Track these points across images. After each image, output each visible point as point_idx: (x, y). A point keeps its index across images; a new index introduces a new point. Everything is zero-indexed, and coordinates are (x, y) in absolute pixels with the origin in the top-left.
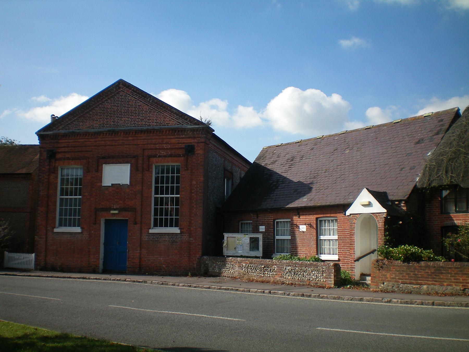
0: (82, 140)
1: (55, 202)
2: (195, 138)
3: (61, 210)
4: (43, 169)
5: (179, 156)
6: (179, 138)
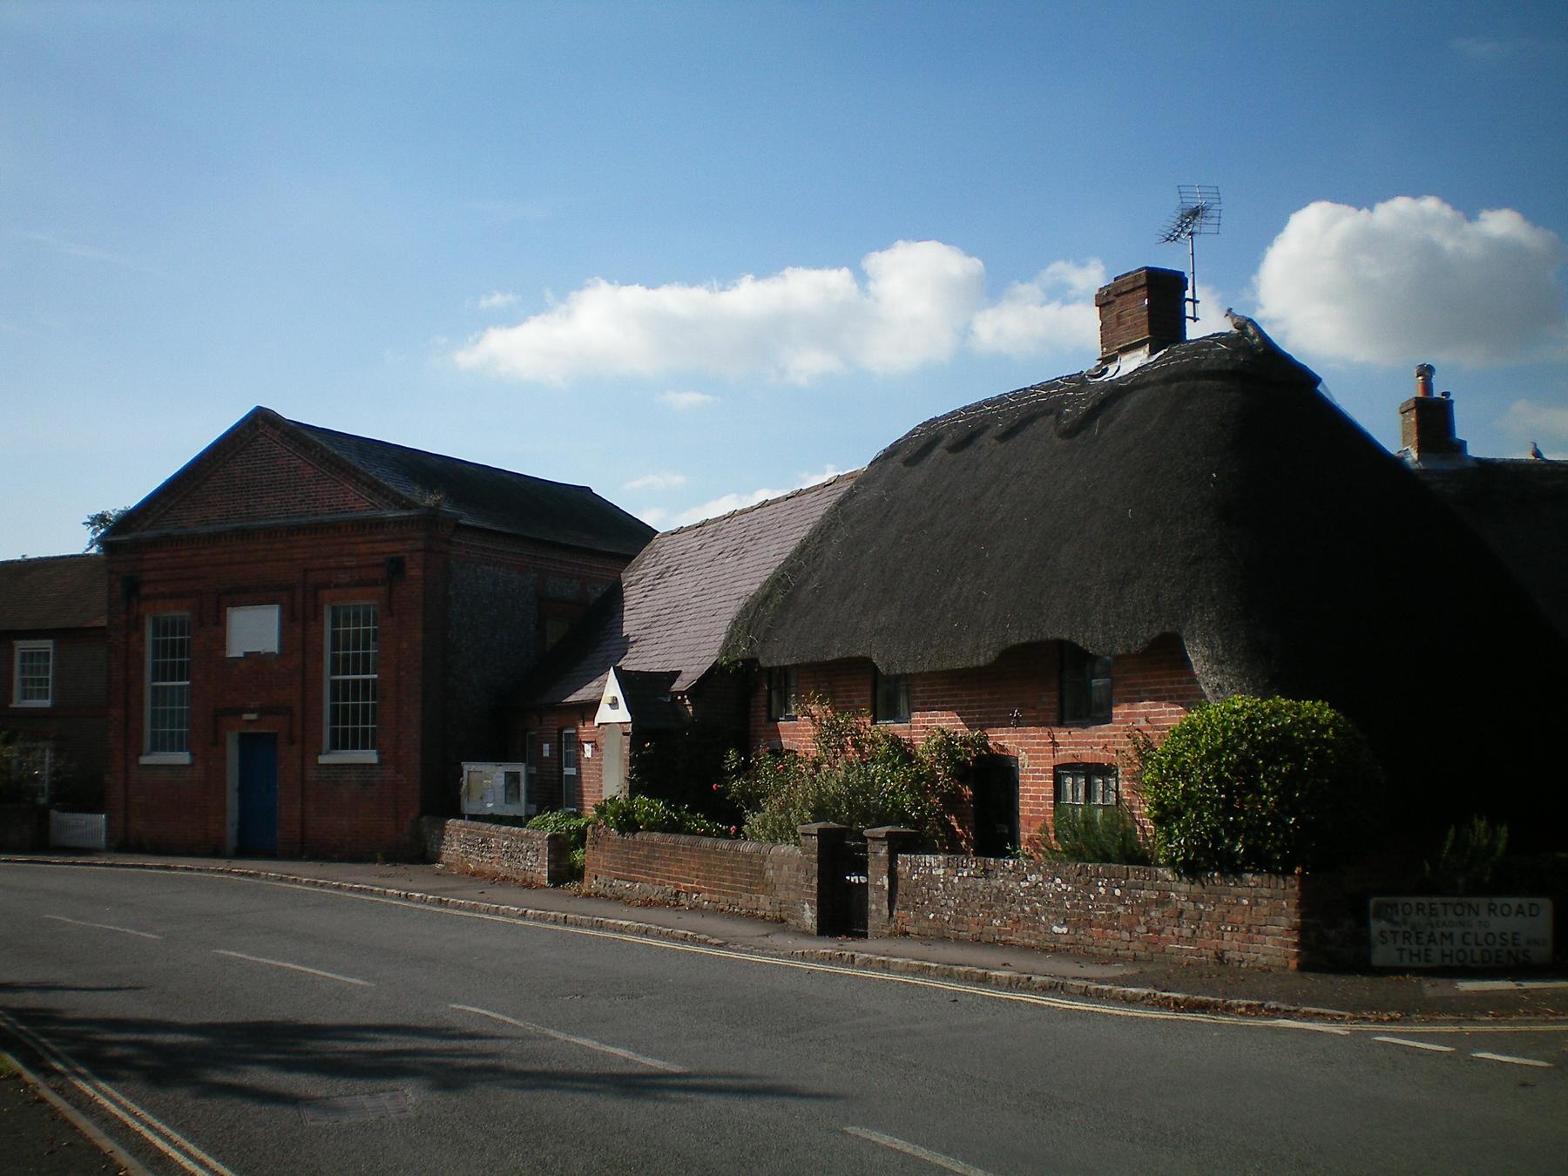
1: (141, 695)
3: (334, 709)
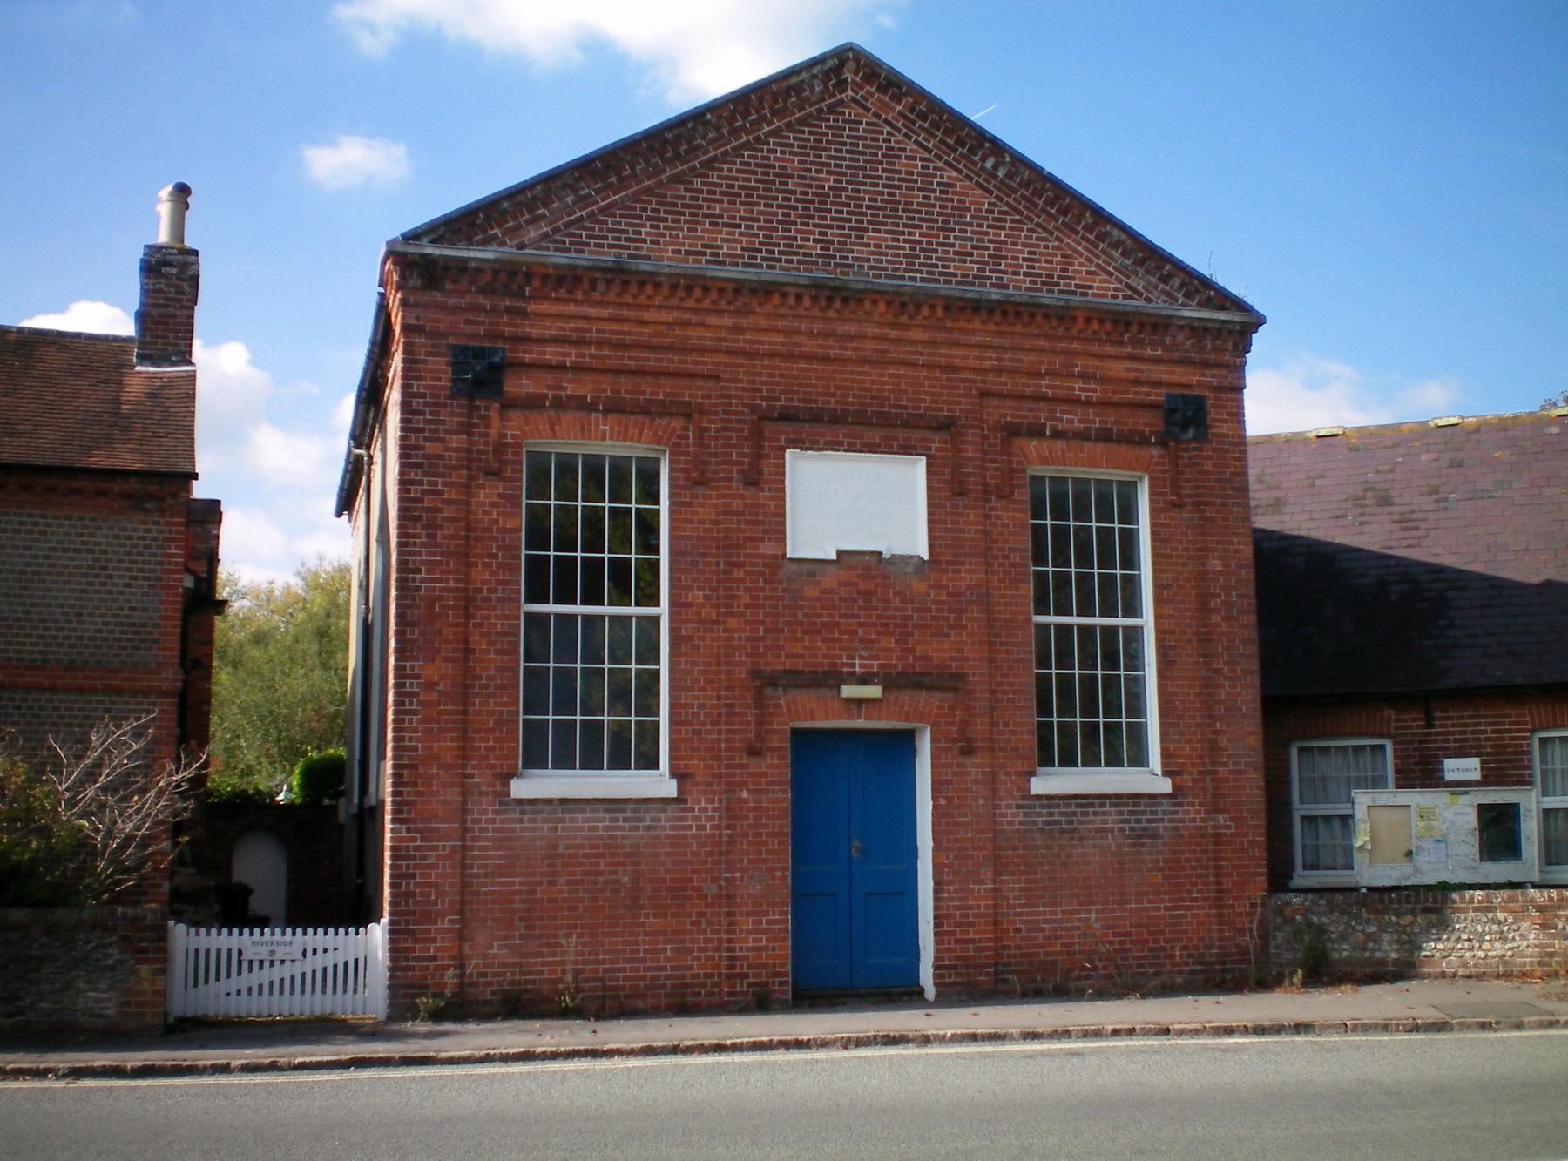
0: (665, 316)
2: (1206, 365)
4: (431, 448)
5: (1144, 441)
6: (1141, 359)
